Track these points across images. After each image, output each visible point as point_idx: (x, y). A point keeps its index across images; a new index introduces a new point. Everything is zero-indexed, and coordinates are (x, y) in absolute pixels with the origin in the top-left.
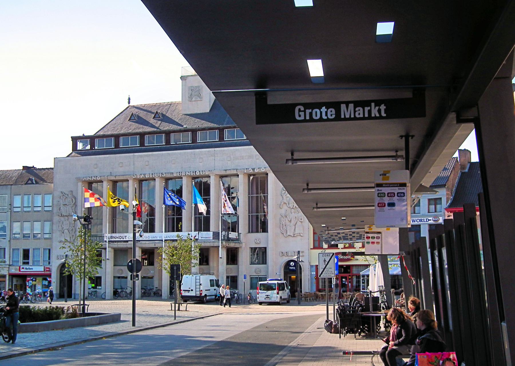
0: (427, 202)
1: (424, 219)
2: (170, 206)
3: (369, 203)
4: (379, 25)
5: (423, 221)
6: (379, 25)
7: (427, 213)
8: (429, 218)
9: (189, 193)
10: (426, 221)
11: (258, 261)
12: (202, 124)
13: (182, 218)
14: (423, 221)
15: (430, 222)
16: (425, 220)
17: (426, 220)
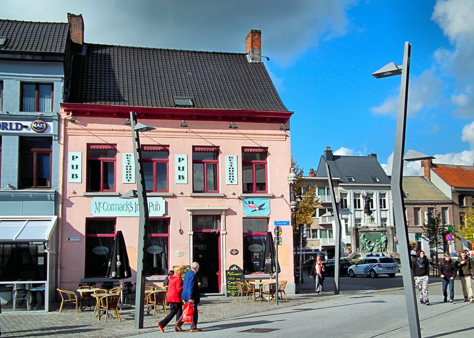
0: (188, 156)
1: (11, 124)
2: (334, 284)
3: (154, 185)
4: (39, 263)
5: (9, 127)
6: (39, 263)
7: (16, 112)
8: (24, 123)
9: (449, 22)
10: (17, 129)
11: (271, 254)
12: (260, 208)
13: (334, 266)
14: (9, 127)
15: (24, 131)
16: (14, 127)
17: (17, 127)
